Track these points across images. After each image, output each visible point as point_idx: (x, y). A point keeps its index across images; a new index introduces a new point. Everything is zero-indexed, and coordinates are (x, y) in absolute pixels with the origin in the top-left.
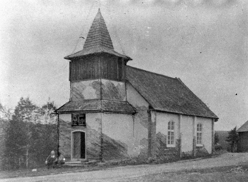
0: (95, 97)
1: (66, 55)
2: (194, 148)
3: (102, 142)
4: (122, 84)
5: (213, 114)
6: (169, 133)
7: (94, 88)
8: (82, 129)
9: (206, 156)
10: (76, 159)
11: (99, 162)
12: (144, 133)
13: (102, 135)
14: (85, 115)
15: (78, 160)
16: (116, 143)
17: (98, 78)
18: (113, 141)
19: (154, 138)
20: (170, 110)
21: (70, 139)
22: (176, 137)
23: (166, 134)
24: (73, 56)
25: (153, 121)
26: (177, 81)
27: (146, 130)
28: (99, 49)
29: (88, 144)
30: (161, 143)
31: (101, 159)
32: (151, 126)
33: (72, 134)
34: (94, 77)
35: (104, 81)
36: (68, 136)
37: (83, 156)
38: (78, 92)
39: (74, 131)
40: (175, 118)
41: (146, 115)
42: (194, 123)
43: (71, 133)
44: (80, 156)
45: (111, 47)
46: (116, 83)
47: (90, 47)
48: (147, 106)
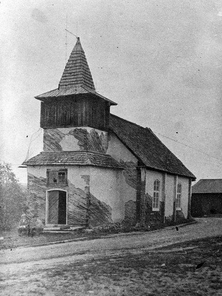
0: (78, 148)
1: (36, 96)
2: (174, 213)
3: (89, 204)
4: (104, 133)
5: (190, 173)
6: (155, 193)
7: (76, 137)
8: (62, 187)
9: (188, 222)
10: (53, 225)
11: (85, 228)
12: (131, 194)
13: (89, 196)
14: (66, 170)
15: (56, 226)
16: (102, 206)
17: (82, 125)
18: (99, 202)
19: (143, 198)
20: (152, 164)
21: (45, 200)
22: (160, 199)
23: (152, 196)
24: (41, 96)
25: (143, 180)
26: (148, 131)
27: (134, 191)
28: (80, 90)
29: (70, 207)
30: (148, 205)
31: (87, 225)
32: (140, 186)
33: (47, 195)
34: (76, 125)
35: (89, 130)
36: (42, 196)
37: (62, 221)
38: (54, 142)
39: (49, 190)
40: (159, 177)
41: (134, 174)
42: (175, 183)
43: (47, 193)
44: (57, 221)
45: (92, 86)
46: (99, 132)
47: (70, 86)
48: (135, 161)
